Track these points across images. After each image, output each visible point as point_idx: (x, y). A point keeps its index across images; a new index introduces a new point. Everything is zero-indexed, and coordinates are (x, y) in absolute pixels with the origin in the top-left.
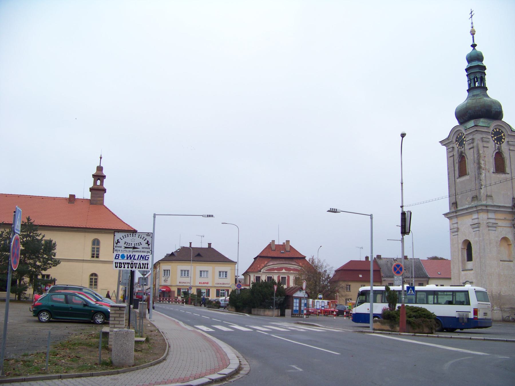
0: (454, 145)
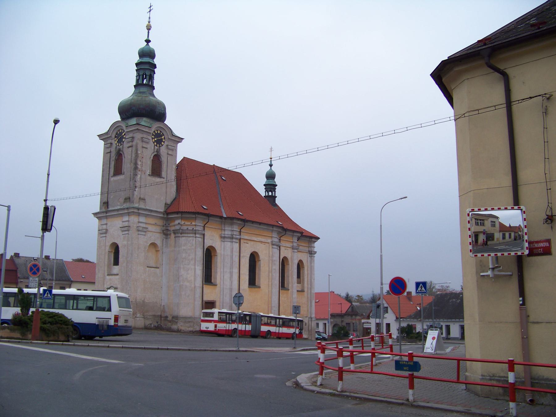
0: (113, 141)
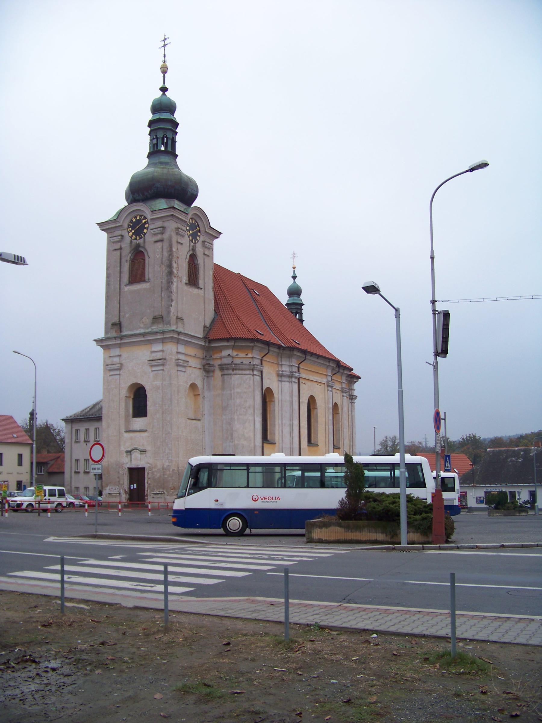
0: (125, 233)
